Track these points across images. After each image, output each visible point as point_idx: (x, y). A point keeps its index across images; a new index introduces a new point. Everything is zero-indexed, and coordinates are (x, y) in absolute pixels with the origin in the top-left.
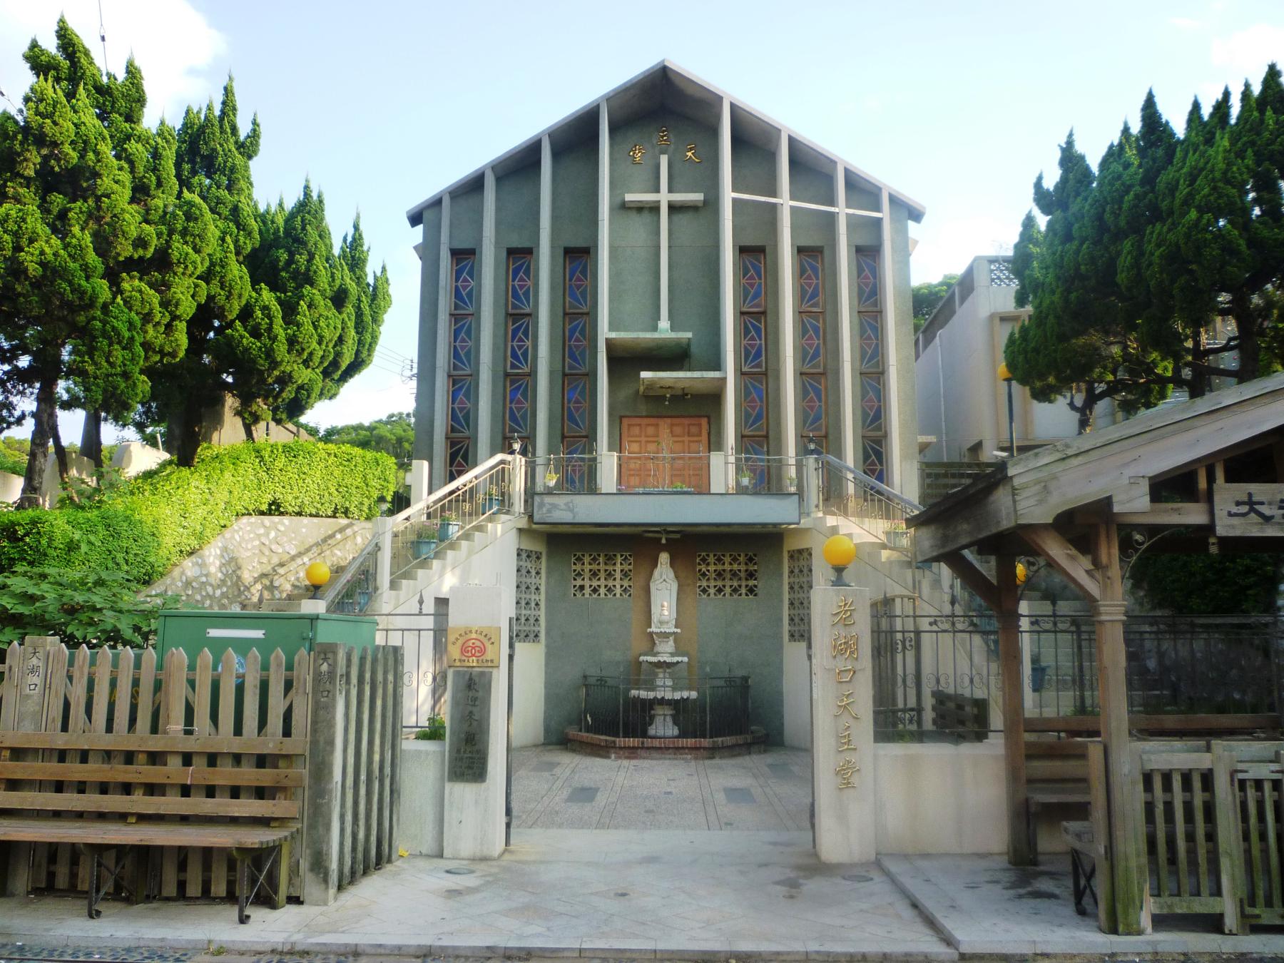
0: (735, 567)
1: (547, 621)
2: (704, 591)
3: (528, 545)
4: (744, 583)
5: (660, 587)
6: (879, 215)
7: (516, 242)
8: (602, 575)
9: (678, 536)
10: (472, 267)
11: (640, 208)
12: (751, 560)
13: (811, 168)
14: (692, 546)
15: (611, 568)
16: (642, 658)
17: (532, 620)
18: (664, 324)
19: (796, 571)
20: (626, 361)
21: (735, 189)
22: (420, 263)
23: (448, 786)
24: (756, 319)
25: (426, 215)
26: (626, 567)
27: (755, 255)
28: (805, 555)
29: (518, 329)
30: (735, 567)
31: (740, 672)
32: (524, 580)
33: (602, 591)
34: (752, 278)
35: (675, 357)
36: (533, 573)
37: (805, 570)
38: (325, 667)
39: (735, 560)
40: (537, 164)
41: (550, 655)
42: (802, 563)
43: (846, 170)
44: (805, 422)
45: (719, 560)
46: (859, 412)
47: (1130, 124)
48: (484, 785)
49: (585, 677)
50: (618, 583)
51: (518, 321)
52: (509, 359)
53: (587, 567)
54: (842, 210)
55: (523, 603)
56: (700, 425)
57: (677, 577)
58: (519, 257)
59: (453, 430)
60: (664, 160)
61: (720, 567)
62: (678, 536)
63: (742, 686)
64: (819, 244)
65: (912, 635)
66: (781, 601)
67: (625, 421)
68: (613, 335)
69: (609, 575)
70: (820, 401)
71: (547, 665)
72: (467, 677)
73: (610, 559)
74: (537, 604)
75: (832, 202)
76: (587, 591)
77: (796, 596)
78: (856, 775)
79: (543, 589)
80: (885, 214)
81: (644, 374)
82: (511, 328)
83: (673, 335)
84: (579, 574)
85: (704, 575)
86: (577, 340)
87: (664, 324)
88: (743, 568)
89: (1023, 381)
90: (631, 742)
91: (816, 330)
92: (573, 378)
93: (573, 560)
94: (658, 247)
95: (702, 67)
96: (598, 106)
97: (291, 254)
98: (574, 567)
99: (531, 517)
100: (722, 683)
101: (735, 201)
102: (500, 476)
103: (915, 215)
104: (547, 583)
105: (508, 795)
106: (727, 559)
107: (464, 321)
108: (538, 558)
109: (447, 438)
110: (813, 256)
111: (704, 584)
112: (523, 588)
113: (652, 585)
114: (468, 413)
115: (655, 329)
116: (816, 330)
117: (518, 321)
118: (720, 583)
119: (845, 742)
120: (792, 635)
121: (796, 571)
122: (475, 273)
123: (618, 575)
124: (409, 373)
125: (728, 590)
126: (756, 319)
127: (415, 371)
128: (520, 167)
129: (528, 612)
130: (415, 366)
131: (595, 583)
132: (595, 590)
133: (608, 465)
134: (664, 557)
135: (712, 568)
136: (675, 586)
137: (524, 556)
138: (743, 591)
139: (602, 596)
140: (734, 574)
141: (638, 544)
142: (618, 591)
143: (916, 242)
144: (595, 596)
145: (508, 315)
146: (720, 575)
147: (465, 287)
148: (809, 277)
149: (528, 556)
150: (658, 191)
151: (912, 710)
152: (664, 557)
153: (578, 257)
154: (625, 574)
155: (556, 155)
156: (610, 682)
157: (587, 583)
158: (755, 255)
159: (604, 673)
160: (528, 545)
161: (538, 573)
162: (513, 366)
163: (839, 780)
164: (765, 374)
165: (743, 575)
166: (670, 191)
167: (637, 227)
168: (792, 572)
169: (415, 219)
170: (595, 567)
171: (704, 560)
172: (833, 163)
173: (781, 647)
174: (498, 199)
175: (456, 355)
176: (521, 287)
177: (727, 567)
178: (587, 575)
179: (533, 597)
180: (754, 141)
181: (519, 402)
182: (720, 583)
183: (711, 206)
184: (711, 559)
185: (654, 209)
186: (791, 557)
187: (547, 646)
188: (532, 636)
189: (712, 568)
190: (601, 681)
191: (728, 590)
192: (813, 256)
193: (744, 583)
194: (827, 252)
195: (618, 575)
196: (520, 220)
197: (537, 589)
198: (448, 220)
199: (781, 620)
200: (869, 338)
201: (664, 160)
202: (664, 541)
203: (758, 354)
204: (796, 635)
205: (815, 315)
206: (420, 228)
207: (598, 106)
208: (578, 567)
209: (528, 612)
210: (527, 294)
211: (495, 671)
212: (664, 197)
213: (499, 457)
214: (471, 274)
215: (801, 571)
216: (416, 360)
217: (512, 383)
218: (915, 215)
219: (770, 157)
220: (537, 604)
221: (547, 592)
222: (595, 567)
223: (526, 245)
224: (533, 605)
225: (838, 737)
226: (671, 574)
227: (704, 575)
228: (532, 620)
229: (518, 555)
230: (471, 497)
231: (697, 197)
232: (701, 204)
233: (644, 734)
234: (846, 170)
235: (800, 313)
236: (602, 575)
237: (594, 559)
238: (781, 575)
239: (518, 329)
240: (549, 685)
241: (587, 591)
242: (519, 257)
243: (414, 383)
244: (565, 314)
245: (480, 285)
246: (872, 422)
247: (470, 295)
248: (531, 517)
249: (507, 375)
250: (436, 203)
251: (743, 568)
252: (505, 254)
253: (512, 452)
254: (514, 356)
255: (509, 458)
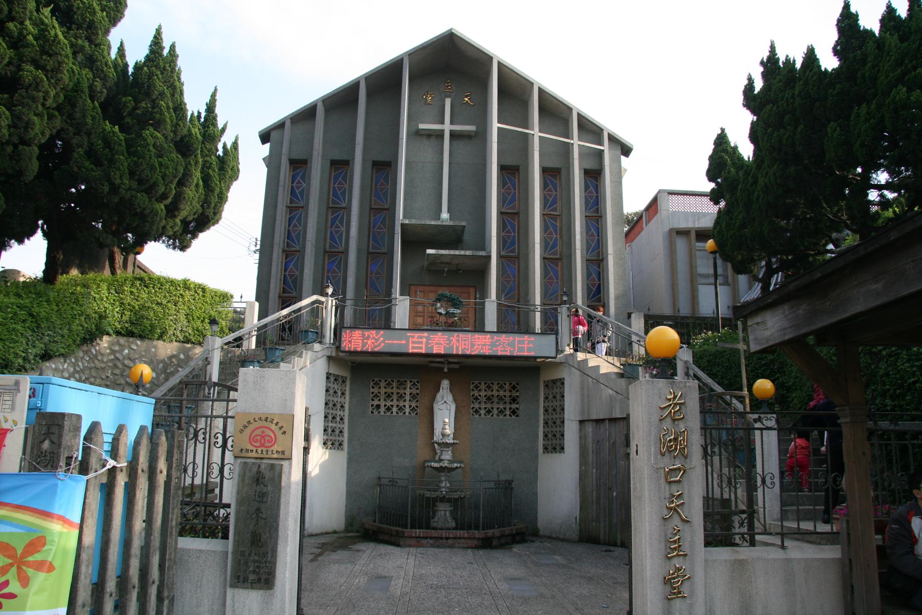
0: (502, 393)
1: (349, 433)
2: (477, 412)
3: (334, 371)
4: (508, 406)
5: (442, 407)
6: (603, 150)
7: (337, 155)
8: (395, 397)
9: (457, 366)
10: (304, 173)
11: (429, 134)
12: (514, 387)
13: (555, 112)
14: (466, 372)
15: (402, 391)
16: (426, 464)
17: (337, 432)
18: (445, 215)
19: (551, 397)
20: (415, 240)
21: (499, 122)
22: (266, 169)
23: (230, 592)
24: (515, 218)
25: (274, 135)
26: (414, 391)
27: (513, 173)
28: (559, 383)
29: (336, 218)
30: (502, 393)
31: (503, 478)
32: (331, 398)
33: (395, 409)
34: (509, 188)
35: (451, 237)
36: (339, 393)
37: (558, 397)
38: (46, 445)
39: (501, 387)
40: (356, 101)
41: (351, 460)
42: (555, 390)
43: (579, 114)
44: (545, 296)
45: (489, 387)
46: (585, 287)
47: (819, 54)
48: (271, 592)
49: (379, 478)
50: (407, 404)
51: (336, 210)
52: (328, 241)
53: (383, 391)
54: (576, 142)
55: (330, 417)
56: (469, 293)
57: (455, 400)
58: (340, 166)
59: (284, 291)
60: (448, 102)
61: (489, 393)
62: (457, 366)
63: (507, 487)
64: (557, 166)
65: (741, 433)
66: (538, 420)
67: (413, 288)
68: (407, 222)
69: (401, 397)
70: (557, 279)
71: (348, 468)
72: (255, 469)
73: (401, 384)
74: (342, 419)
75: (568, 135)
76: (382, 409)
77: (550, 417)
78: (687, 584)
79: (347, 406)
80: (606, 147)
81: (429, 251)
82: (330, 217)
83: (451, 223)
84: (376, 396)
85: (476, 399)
86: (379, 228)
87: (445, 215)
88: (508, 394)
89: (726, 258)
90: (418, 532)
91: (555, 227)
92: (376, 255)
93: (372, 384)
94: (442, 163)
95: (480, 34)
96: (402, 59)
97: (137, 101)
98: (372, 390)
99: (338, 348)
100: (492, 485)
101: (499, 128)
102: (316, 310)
103: (626, 150)
104: (350, 403)
105: (299, 599)
106: (495, 387)
107: (296, 209)
108: (344, 382)
109: (279, 297)
110: (554, 175)
111: (477, 406)
112: (331, 405)
113: (435, 406)
114: (296, 278)
115: (438, 218)
116: (555, 227)
117: (336, 210)
118: (489, 406)
119: (673, 548)
120: (546, 449)
121: (551, 397)
122: (306, 177)
123: (408, 398)
124: (254, 248)
125: (495, 411)
126: (515, 218)
127: (258, 247)
128: (343, 101)
129: (334, 425)
130: (259, 243)
131: (389, 404)
132: (389, 409)
133: (402, 309)
134: (445, 383)
135: (483, 393)
136: (453, 407)
137: (332, 379)
138: (508, 412)
139: (394, 413)
140: (500, 399)
141: (426, 371)
142: (407, 410)
143: (626, 170)
144: (388, 414)
145: (328, 208)
146: (489, 399)
147: (298, 188)
148: (550, 190)
149: (336, 380)
150: (442, 122)
151: (743, 512)
152: (445, 383)
153: (383, 168)
154: (413, 397)
155: (369, 95)
156: (400, 483)
157: (382, 403)
158: (513, 173)
159: (395, 476)
160: (334, 371)
161: (343, 394)
162: (331, 246)
163: (668, 588)
164: (518, 258)
165: (507, 400)
166: (452, 123)
167: (426, 151)
168: (546, 398)
169: (265, 137)
170: (389, 390)
171: (477, 387)
172: (570, 109)
173: (537, 456)
174: (326, 125)
175: (289, 236)
176: (340, 189)
177: (495, 393)
178: (383, 397)
179: (339, 413)
180: (515, 90)
181: (334, 272)
182: (489, 406)
183: (481, 136)
184: (483, 387)
185: (440, 135)
186: (547, 386)
187: (349, 453)
188: (337, 444)
189: (483, 393)
190: (393, 482)
191: (495, 411)
192: (554, 175)
193: (508, 406)
194: (563, 172)
195: (408, 398)
196: (344, 142)
197: (342, 406)
198: (290, 140)
199: (537, 436)
200: (592, 235)
201: (448, 102)
202: (446, 370)
203: (513, 243)
204: (550, 448)
205: (554, 218)
206: (268, 144)
207: (402, 59)
208: (376, 390)
209: (334, 425)
210: (343, 194)
211: (285, 464)
212: (447, 127)
213: (315, 297)
214: (303, 178)
215: (555, 397)
216: (259, 239)
217: (330, 257)
218: (626, 150)
219: (525, 103)
220: (342, 419)
221: (350, 409)
222: (389, 390)
223: (345, 158)
224: (338, 419)
225: (668, 542)
226: (450, 398)
227: (476, 399)
228: (337, 432)
229: (328, 378)
230: (290, 329)
231: (471, 128)
232: (473, 134)
233: (428, 527)
234: (579, 114)
235: (543, 215)
236: (395, 397)
237: (389, 384)
238: (538, 400)
239: (336, 218)
240: (349, 494)
241: (382, 409)
242: (340, 166)
243: (257, 256)
244: (371, 209)
245: (309, 185)
246: (594, 295)
247: (302, 193)
248: (338, 348)
249: (326, 252)
250: (280, 126)
251: (508, 394)
252: (329, 164)
253: (326, 295)
254: (332, 238)
255: (323, 299)
